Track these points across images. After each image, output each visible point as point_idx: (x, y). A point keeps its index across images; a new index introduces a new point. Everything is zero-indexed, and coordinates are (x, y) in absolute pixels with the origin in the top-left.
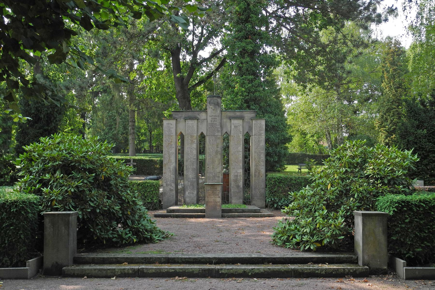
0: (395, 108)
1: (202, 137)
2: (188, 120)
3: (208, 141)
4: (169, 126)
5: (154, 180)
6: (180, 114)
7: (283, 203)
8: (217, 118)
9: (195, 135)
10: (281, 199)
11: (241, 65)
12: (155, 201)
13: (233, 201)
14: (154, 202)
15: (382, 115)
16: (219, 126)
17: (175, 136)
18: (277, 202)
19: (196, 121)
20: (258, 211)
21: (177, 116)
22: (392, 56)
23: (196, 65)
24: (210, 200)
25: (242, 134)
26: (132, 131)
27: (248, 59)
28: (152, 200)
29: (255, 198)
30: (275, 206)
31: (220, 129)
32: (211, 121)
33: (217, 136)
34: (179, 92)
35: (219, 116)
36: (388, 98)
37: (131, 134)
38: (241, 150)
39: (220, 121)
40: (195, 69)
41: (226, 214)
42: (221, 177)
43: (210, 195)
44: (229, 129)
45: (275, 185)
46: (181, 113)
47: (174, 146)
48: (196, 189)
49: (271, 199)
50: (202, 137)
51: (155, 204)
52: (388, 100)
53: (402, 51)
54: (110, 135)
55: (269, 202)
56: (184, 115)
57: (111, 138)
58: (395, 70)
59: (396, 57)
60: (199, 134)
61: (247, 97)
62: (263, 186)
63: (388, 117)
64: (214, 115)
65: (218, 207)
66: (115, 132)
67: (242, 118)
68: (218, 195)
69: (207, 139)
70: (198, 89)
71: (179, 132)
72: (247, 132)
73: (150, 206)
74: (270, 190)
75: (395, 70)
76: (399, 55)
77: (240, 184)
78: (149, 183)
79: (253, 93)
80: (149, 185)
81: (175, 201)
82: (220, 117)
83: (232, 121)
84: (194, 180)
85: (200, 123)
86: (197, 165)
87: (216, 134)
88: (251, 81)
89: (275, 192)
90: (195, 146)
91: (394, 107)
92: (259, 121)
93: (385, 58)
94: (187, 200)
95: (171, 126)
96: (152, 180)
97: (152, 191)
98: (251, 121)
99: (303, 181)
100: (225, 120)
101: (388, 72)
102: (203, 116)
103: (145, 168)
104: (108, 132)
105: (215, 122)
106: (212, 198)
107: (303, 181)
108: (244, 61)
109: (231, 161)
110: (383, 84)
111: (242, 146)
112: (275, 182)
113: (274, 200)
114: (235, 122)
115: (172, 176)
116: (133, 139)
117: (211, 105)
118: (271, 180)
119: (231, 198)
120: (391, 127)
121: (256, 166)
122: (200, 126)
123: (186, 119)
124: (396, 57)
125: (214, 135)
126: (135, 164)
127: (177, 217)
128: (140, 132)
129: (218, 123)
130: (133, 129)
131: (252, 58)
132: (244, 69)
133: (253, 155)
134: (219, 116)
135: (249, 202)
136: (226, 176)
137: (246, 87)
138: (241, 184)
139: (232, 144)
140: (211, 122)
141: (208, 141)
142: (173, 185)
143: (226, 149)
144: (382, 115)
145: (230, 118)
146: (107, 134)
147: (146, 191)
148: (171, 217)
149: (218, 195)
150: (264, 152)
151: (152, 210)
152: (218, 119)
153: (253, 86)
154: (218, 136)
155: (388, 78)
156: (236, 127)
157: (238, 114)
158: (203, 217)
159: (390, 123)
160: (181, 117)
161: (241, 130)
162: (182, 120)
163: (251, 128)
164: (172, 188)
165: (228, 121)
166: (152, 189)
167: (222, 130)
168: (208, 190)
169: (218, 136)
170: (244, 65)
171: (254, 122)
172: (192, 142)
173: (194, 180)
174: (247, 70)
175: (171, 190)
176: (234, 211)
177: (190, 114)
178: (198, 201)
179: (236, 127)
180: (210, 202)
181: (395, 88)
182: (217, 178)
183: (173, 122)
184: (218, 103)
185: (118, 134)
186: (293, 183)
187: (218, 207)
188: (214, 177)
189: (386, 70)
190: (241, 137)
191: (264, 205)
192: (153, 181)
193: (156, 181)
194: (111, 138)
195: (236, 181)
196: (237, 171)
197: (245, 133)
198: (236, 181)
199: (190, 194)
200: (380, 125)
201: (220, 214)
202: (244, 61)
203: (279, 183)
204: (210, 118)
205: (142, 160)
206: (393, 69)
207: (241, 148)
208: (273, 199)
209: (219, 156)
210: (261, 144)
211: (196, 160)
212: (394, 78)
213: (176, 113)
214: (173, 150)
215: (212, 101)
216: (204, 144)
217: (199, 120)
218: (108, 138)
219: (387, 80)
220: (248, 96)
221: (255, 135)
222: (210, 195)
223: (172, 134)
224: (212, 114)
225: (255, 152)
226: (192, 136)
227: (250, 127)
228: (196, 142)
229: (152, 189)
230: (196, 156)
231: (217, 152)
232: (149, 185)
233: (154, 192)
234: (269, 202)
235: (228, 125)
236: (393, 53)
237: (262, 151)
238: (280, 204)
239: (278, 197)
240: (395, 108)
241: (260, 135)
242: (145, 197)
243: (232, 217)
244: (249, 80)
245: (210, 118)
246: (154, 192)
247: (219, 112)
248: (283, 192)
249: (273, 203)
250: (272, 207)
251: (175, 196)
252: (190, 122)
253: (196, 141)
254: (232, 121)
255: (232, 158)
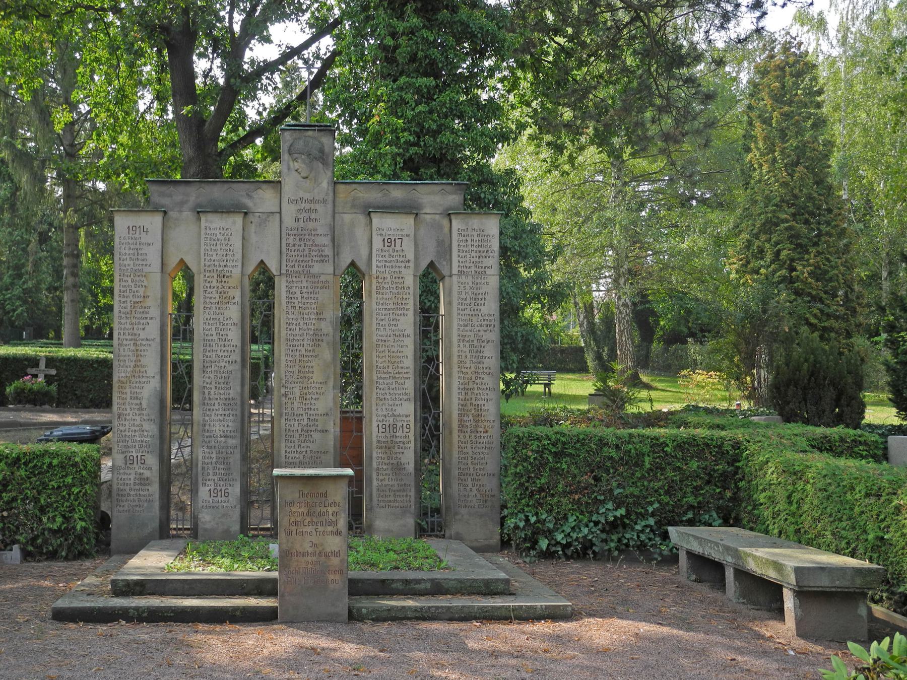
0: (787, 221)
1: (263, 284)
2: (211, 217)
3: (284, 295)
4: (138, 238)
5: (81, 441)
6: (178, 194)
7: (574, 535)
8: (317, 206)
9: (237, 271)
10: (565, 518)
11: (389, 41)
12: (80, 525)
13: (379, 524)
14: (74, 528)
15: (748, 241)
16: (326, 240)
17: (157, 277)
18: (550, 532)
19: (239, 219)
20: (501, 587)
21: (166, 201)
22: (777, 77)
23: (243, 82)
24: (298, 547)
25: (411, 271)
26: (71, 280)
27: (415, 21)
28: (66, 519)
29: (463, 511)
30: (544, 544)
31: (328, 251)
32: (297, 220)
33: (319, 275)
34: (190, 161)
35: (324, 201)
36: (767, 192)
37: (67, 289)
38: (410, 330)
39: (329, 219)
40: (238, 93)
41: (365, 604)
42: (333, 428)
43: (297, 523)
44: (364, 252)
45: (541, 465)
46: (182, 189)
47: (155, 312)
48: (237, 475)
49: (527, 520)
50: (263, 284)
51: (79, 538)
52: (768, 199)
53: (806, 64)
54: (17, 291)
55: (517, 527)
56: (195, 194)
57: (19, 298)
58: (787, 116)
59: (789, 81)
60: (250, 268)
61: (413, 150)
62: (491, 464)
63: (767, 245)
64: (307, 196)
65: (331, 577)
66: (30, 284)
67: (411, 209)
68: (333, 523)
69: (281, 286)
70: (247, 153)
71: (173, 261)
72: (432, 265)
73: (61, 545)
74: (522, 485)
75: (787, 116)
76: (799, 75)
77: (403, 461)
78: (56, 455)
79: (435, 133)
80: (55, 462)
81: (156, 524)
82: (330, 206)
83: (376, 220)
84: (231, 442)
85: (252, 228)
86: (243, 385)
87: (316, 268)
88: (426, 96)
89: (541, 490)
90: (233, 313)
91: (784, 216)
92: (475, 222)
93: (756, 85)
94: (206, 519)
95: (145, 238)
96: (71, 440)
97: (69, 487)
98: (445, 222)
99: (646, 449)
100: (347, 218)
101: (767, 121)
102: (265, 200)
103: (84, 385)
104: (12, 284)
105: (311, 225)
106: (308, 538)
107: (646, 449)
108: (401, 26)
109: (370, 369)
110: (750, 155)
111: (411, 313)
112: (540, 452)
113: (538, 521)
114: (384, 223)
115: (146, 426)
116: (72, 301)
117: (295, 160)
118: (525, 446)
119: (370, 509)
120: (775, 271)
121: (466, 389)
122: (254, 238)
123: (199, 212)
124: (789, 81)
125: (308, 275)
126: (53, 372)
127: (154, 616)
128: (99, 285)
129: (322, 227)
130: (74, 275)
131: (429, 20)
132: (402, 55)
133: (455, 349)
134: (324, 201)
135: (440, 525)
136: (352, 425)
137: (410, 114)
138: (409, 458)
139: (372, 305)
140: (295, 225)
141: (284, 295)
142: (153, 461)
143: (351, 324)
144: (748, 241)
145: (369, 210)
146: (7, 289)
147: (45, 486)
148: (129, 619)
149: (333, 523)
150: (494, 336)
151: (66, 559)
152: (323, 212)
153: (431, 112)
154: (323, 278)
155: (766, 138)
156: (389, 242)
157: (397, 194)
158: (267, 617)
159: (773, 262)
160: (182, 203)
161: (410, 256)
162: (187, 214)
163: (445, 248)
164: (147, 474)
165: (362, 218)
166: (69, 480)
167: (336, 254)
168: (291, 504)
169: (323, 278)
170: (403, 41)
171: (456, 223)
172: (225, 300)
173: (231, 442)
174: (413, 58)
175: (143, 481)
176: (399, 586)
177: (216, 192)
178: (248, 531)
179: (389, 242)
180: (298, 554)
181: (786, 165)
182: (316, 436)
183: (154, 222)
184: (322, 151)
185: (37, 288)
186: (611, 458)
187: (331, 577)
188: (307, 431)
189: (759, 117)
190: (410, 281)
191: (496, 540)
192: (75, 447)
193: (86, 448)
194: (19, 298)
195: (389, 447)
196: (391, 408)
197: (424, 264)
198: (389, 447)
199: (216, 498)
200: (742, 265)
201: (343, 604)
202: (401, 26)
203: (558, 456)
204: (293, 208)
205: (74, 360)
206: (781, 114)
207: (408, 322)
208: (533, 519)
209: (327, 354)
210: (484, 310)
211: (238, 367)
212: (783, 136)
213: (163, 188)
214: (152, 330)
215: (300, 144)
216: (271, 307)
217: (250, 217)
218: (10, 299)
219: (765, 143)
220: (416, 144)
221: (461, 273)
222: (297, 523)
223: (146, 269)
224: (301, 194)
225: (462, 339)
226: (223, 277)
227: (440, 243)
228: (238, 299)
229: (69, 480)
230: (238, 350)
231: (317, 338)
232: (55, 462)
233: (75, 490)
234: (517, 527)
235: (361, 233)
236: (782, 69)
237: (486, 336)
238: (559, 537)
239: (551, 511)
240: (787, 221)
241: (481, 273)
242: (43, 510)
243: (394, 619)
244: (418, 91)
245: (293, 208)
246: (75, 490)
247: (325, 184)
248: (571, 493)
249: (534, 533)
250: (529, 549)
251: (157, 504)
252: (215, 223)
253: (237, 294)
254: (376, 220)
255: (371, 358)
